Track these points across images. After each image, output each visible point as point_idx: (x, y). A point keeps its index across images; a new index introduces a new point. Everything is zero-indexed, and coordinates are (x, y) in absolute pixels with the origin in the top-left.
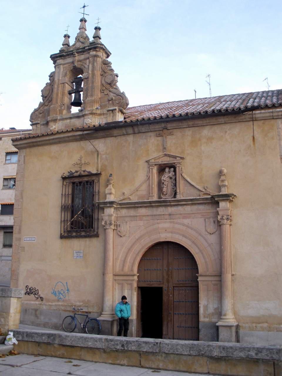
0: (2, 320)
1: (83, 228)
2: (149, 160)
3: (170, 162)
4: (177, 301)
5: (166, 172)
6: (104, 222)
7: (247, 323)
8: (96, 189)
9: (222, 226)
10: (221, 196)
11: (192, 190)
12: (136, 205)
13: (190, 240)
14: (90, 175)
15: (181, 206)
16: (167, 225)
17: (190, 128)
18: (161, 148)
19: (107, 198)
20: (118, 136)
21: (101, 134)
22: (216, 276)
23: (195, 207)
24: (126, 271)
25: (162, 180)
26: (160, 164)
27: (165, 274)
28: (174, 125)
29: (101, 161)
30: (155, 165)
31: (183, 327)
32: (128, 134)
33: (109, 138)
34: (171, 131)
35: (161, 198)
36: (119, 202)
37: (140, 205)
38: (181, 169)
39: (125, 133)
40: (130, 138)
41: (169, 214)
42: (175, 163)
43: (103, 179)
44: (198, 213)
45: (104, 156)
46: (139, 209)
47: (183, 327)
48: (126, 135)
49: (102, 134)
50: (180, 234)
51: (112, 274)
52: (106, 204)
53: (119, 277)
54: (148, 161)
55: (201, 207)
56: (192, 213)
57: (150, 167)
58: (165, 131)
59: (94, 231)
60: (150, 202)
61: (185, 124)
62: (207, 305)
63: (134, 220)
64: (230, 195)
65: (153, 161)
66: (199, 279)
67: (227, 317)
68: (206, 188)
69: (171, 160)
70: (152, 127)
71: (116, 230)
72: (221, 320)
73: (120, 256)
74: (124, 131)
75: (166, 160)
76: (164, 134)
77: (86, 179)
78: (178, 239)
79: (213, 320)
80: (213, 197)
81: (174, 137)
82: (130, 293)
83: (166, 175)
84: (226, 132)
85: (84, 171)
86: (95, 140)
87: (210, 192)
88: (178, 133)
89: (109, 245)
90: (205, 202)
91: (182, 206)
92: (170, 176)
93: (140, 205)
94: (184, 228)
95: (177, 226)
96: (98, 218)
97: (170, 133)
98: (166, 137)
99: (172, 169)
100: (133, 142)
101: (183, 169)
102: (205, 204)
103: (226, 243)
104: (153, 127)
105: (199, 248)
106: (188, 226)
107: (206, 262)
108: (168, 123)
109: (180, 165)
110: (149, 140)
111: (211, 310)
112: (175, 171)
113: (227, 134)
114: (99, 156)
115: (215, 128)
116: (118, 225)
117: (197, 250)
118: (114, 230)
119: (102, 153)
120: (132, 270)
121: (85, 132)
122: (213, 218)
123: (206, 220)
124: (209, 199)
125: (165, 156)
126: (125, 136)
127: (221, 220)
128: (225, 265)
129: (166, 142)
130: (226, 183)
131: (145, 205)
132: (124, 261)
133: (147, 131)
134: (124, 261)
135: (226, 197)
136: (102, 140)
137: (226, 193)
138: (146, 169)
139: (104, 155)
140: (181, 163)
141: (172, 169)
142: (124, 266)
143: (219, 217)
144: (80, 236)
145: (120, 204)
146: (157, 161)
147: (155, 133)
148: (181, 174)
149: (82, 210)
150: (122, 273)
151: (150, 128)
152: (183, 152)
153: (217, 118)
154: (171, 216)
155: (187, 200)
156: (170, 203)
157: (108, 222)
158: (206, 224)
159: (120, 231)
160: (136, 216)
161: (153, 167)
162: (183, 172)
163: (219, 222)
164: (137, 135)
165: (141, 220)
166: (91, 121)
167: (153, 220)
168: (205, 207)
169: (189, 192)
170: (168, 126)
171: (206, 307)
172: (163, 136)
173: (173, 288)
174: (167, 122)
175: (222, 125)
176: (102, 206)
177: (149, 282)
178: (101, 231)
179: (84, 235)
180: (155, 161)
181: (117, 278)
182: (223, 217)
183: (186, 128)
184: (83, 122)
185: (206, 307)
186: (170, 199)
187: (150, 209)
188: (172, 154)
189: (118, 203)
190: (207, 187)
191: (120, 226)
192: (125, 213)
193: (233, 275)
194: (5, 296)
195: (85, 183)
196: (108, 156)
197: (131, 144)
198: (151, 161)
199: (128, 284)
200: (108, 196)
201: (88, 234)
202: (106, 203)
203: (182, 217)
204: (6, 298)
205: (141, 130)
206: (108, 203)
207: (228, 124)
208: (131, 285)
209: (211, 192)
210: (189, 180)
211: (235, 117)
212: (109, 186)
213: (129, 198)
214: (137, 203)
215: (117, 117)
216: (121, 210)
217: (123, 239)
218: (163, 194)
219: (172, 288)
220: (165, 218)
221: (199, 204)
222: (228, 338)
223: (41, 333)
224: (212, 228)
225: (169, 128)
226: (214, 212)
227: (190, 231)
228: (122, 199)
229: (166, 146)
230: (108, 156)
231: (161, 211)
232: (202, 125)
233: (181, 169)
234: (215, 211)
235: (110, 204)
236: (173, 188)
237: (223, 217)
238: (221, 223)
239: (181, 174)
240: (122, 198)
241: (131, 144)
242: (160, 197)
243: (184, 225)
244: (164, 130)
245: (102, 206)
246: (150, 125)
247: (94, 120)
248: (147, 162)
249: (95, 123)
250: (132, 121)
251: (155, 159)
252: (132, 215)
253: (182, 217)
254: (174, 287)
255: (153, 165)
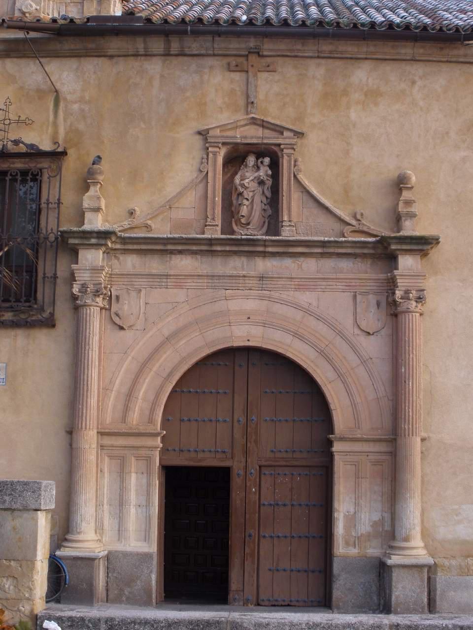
0: (8, 584)
1: (10, 301)
2: (208, 131)
3: (265, 141)
4: (271, 505)
5: (246, 166)
6: (79, 286)
7: (454, 557)
8: (49, 192)
9: (400, 317)
10: (406, 241)
11: (323, 220)
12: (170, 247)
13: (314, 346)
14: (34, 153)
15: (290, 257)
16: (251, 305)
17: (323, 61)
18: (242, 102)
19: (86, 221)
20: (119, 56)
21: (70, 44)
22: (380, 440)
23: (329, 264)
24: (134, 423)
25: (240, 187)
26: (237, 144)
27: (238, 435)
28: (282, 46)
29: (65, 120)
30: (224, 144)
31: (284, 570)
32: (148, 55)
33: (91, 59)
34: (269, 60)
35: (233, 232)
36: (123, 235)
37: (180, 248)
38: (295, 161)
39: (142, 51)
40: (155, 67)
41: (260, 277)
42: (279, 145)
43: (71, 166)
44: (336, 279)
45: (76, 107)
46: (173, 256)
47: (284, 570)
48: (143, 58)
49: (72, 47)
50: (287, 331)
51: (95, 431)
52: (89, 238)
53: (114, 438)
54: (203, 133)
55: (345, 264)
56: (323, 277)
57: (210, 149)
58: (253, 58)
59: (42, 309)
60: (210, 240)
61: (311, 48)
62: (355, 513)
63: (161, 287)
64: (430, 241)
65: (217, 132)
66: (337, 447)
67: (412, 544)
68: (359, 217)
69: (267, 135)
70: (220, 44)
71: (106, 309)
72: (397, 553)
73: (118, 382)
74: (139, 44)
75: (254, 135)
76: (250, 67)
77: (19, 165)
78: (281, 342)
79: (368, 551)
80: (383, 241)
81: (277, 77)
82: (144, 481)
83: (247, 174)
84: (414, 83)
85: (16, 142)
86: (48, 59)
87: (369, 228)
88: (288, 70)
89: (90, 352)
90: (358, 251)
91: (294, 259)
92: (262, 178)
93: (180, 248)
94: (299, 315)
95: (280, 310)
96: (55, 274)
97: (268, 66)
98: (255, 75)
99: (267, 160)
100: (162, 76)
101: (298, 163)
102: (355, 256)
103: (413, 358)
104: (223, 45)
105: (335, 369)
106: (307, 311)
107: (354, 405)
108: (265, 40)
109: (218, 150)
110: (206, 77)
111: (364, 526)
112: (275, 166)
113: (416, 88)
114: (62, 105)
115: (387, 67)
116: (113, 298)
117: (331, 374)
118: (101, 309)
119: (69, 97)
120: (151, 421)
121: (33, 35)
122: (375, 293)
123: (359, 297)
124: (370, 246)
125: (251, 124)
126: (139, 58)
127: (401, 301)
128: (409, 415)
129: (256, 86)
130: (414, 209)
131: (194, 248)
132: (130, 395)
133: (203, 52)
134: (130, 395)
135: (418, 244)
136: (73, 63)
137: (417, 233)
138: (198, 154)
139: (76, 102)
140: (295, 147)
141: (267, 160)
142: (126, 409)
143: (397, 292)
144: (27, 322)
145: (124, 241)
146: (229, 133)
147: (225, 61)
148: (295, 176)
149: (6, 250)
150: (123, 428)
151: (216, 46)
152: (300, 118)
153: (397, 43)
154: (264, 282)
155: (310, 244)
156: (265, 246)
157: (91, 288)
158: (356, 309)
159: (120, 312)
160: (167, 276)
161: (217, 150)
162: (300, 171)
163: (74, 298)
164: (175, 61)
165: (181, 287)
166: (38, 8)
167: (214, 288)
168: (354, 264)
169: (312, 224)
170: (266, 46)
171: (352, 521)
172: (247, 72)
173: (258, 468)
174: (265, 35)
175: (404, 62)
176: (76, 241)
177: (193, 455)
178: (62, 310)
179: (10, 321)
180: (225, 134)
181: (107, 441)
182: (407, 292)
183: (311, 57)
184: (10, 5)
185: (352, 521)
186: (259, 237)
187: (205, 259)
188: (269, 119)
189: (120, 237)
190: (362, 215)
191: (121, 299)
192: (134, 267)
193: (423, 440)
194: (14, 506)
195: (17, 175)
196: (86, 108)
197: (156, 83)
198: (211, 133)
199: (138, 458)
200: (88, 216)
201: (23, 316)
202: (88, 235)
203: (293, 287)
204: (16, 513)
205: (189, 47)
206: (95, 235)
207: (421, 63)
208: (149, 460)
209: (372, 227)
210: (315, 192)
211: (442, 49)
212: (92, 189)
213: (148, 227)
214: (171, 241)
215: (112, 6)
216: (121, 257)
217: (128, 335)
218: (238, 222)
219: (256, 469)
220: (247, 285)
221: (339, 255)
222: (415, 595)
223: (166, 620)
224: (372, 318)
225: (265, 53)
226: (379, 279)
227: (312, 322)
228: (126, 227)
229: (256, 97)
230: (86, 108)
231: (236, 265)
232: (354, 56)
233: (295, 161)
234: (382, 276)
235: (98, 238)
236: (264, 210)
237: (407, 292)
238: (78, 302)
239: (295, 176)
240: (126, 224)
241: (156, 83)
242: (227, 228)
243: (297, 307)
244: (250, 57)
245: (76, 241)
246: (217, 38)
247: (44, 6)
248: (199, 133)
249: (49, 15)
250: (169, 20)
251: (223, 127)
252: (154, 271)
253: (293, 287)
254: (263, 469)
255: (219, 143)
